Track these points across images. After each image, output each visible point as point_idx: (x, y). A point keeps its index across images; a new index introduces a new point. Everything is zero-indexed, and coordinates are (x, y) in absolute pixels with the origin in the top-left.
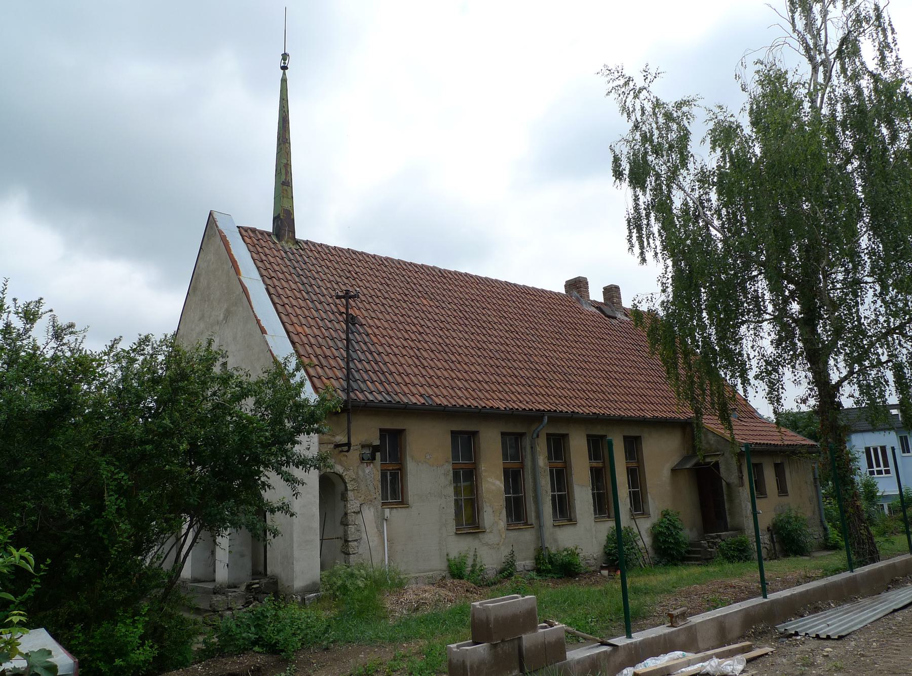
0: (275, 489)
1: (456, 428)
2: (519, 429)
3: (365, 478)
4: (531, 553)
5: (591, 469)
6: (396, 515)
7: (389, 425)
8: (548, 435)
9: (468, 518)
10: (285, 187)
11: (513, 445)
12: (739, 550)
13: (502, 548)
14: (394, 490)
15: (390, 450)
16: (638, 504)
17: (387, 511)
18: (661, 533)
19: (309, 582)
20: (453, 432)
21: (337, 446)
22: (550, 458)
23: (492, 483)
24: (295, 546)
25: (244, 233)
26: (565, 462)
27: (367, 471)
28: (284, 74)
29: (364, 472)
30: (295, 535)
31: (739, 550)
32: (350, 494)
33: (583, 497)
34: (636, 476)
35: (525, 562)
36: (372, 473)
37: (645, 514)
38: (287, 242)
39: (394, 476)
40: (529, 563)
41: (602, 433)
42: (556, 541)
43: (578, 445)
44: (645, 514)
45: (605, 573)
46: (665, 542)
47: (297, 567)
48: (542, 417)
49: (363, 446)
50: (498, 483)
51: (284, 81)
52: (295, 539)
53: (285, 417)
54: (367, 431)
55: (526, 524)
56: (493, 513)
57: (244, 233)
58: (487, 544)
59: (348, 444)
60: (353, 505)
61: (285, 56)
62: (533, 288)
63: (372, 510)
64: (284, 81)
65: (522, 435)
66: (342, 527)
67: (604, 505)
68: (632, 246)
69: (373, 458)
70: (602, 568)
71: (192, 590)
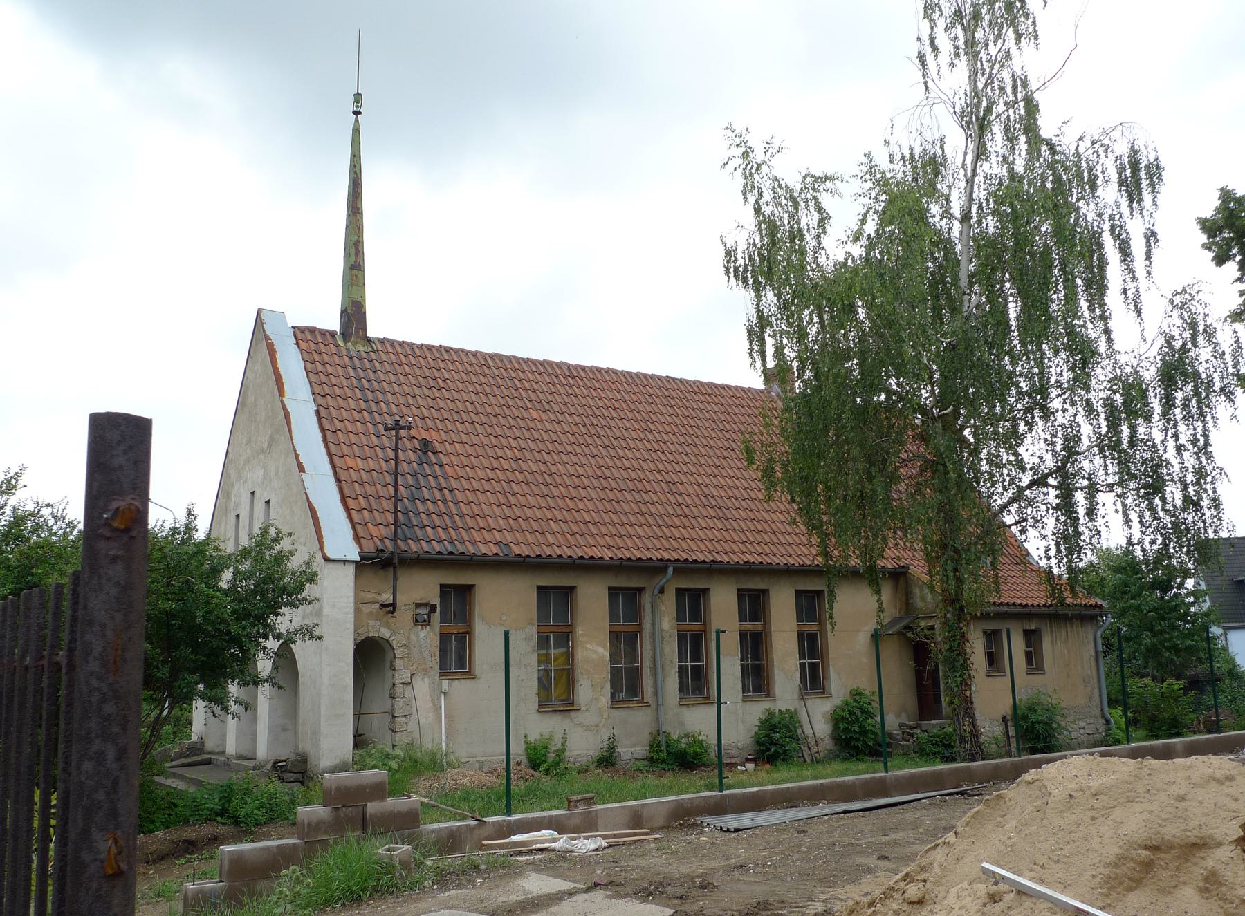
2: (634, 583)
3: (418, 644)
4: (645, 738)
5: (743, 635)
6: (460, 687)
8: (680, 592)
9: (557, 693)
10: (355, 272)
11: (625, 602)
12: (945, 746)
13: (603, 730)
14: (456, 657)
15: (458, 600)
16: (813, 678)
17: (445, 684)
18: (844, 718)
19: (338, 761)
20: (539, 588)
21: (383, 606)
22: (680, 617)
23: (593, 650)
24: (323, 720)
25: (299, 335)
26: (705, 624)
28: (357, 121)
29: (417, 635)
30: (323, 709)
31: (945, 746)
32: (398, 663)
33: (730, 669)
34: (812, 645)
35: (632, 749)
36: (427, 639)
37: (825, 694)
38: (355, 344)
40: (641, 750)
41: (764, 587)
42: (682, 724)
43: (723, 604)
44: (825, 694)
45: (750, 766)
46: (846, 730)
47: (325, 744)
48: (666, 568)
49: (418, 606)
50: (600, 650)
51: (356, 131)
52: (323, 713)
55: (641, 701)
56: (592, 689)
57: (299, 335)
58: (581, 725)
59: (393, 605)
60: (402, 675)
61: (358, 98)
62: (709, 384)
63: (427, 681)
64: (356, 131)
66: (389, 701)
67: (757, 678)
68: (754, 361)
70: (748, 760)
71: (687, 788)
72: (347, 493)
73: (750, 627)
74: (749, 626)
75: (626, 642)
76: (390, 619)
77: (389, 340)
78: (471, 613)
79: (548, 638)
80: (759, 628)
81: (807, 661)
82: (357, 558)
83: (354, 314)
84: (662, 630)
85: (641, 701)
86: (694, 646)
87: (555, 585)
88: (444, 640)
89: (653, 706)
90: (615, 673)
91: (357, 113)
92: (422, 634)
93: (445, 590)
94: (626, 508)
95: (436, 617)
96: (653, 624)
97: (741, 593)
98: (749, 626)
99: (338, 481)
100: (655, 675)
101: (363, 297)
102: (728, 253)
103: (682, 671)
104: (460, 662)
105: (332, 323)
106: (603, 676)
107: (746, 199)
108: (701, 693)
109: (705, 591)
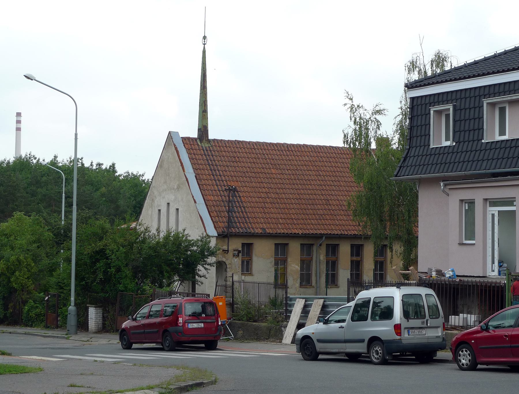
0: (201, 269)
1: (277, 242)
5: (352, 262)
7: (246, 241)
8: (328, 245)
11: (307, 249)
15: (247, 250)
21: (223, 250)
22: (327, 254)
23: (294, 267)
27: (236, 260)
36: (237, 261)
39: (248, 263)
49: (234, 250)
50: (297, 267)
51: (204, 52)
53: (204, 252)
54: (236, 244)
59: (228, 251)
61: (205, 38)
64: (204, 52)
65: (313, 245)
69: (238, 256)
72: (210, 210)
73: (355, 259)
74: (355, 258)
75: (306, 265)
76: (226, 255)
77: (216, 140)
78: (252, 253)
79: (278, 262)
80: (359, 259)
81: (378, 272)
82: (217, 235)
83: (203, 130)
84: (320, 260)
85: (311, 285)
86: (332, 266)
87: (281, 244)
88: (243, 262)
89: (316, 287)
90: (302, 275)
91: (204, 44)
92: (236, 260)
93: (243, 245)
94: (308, 212)
95: (240, 254)
96: (317, 257)
97: (352, 246)
98: (355, 258)
99: (207, 205)
100: (316, 276)
101: (207, 123)
102: (345, 136)
103: (327, 275)
104: (247, 270)
105: (194, 134)
106: (298, 276)
107: (351, 119)
108: (334, 283)
109: (338, 245)
